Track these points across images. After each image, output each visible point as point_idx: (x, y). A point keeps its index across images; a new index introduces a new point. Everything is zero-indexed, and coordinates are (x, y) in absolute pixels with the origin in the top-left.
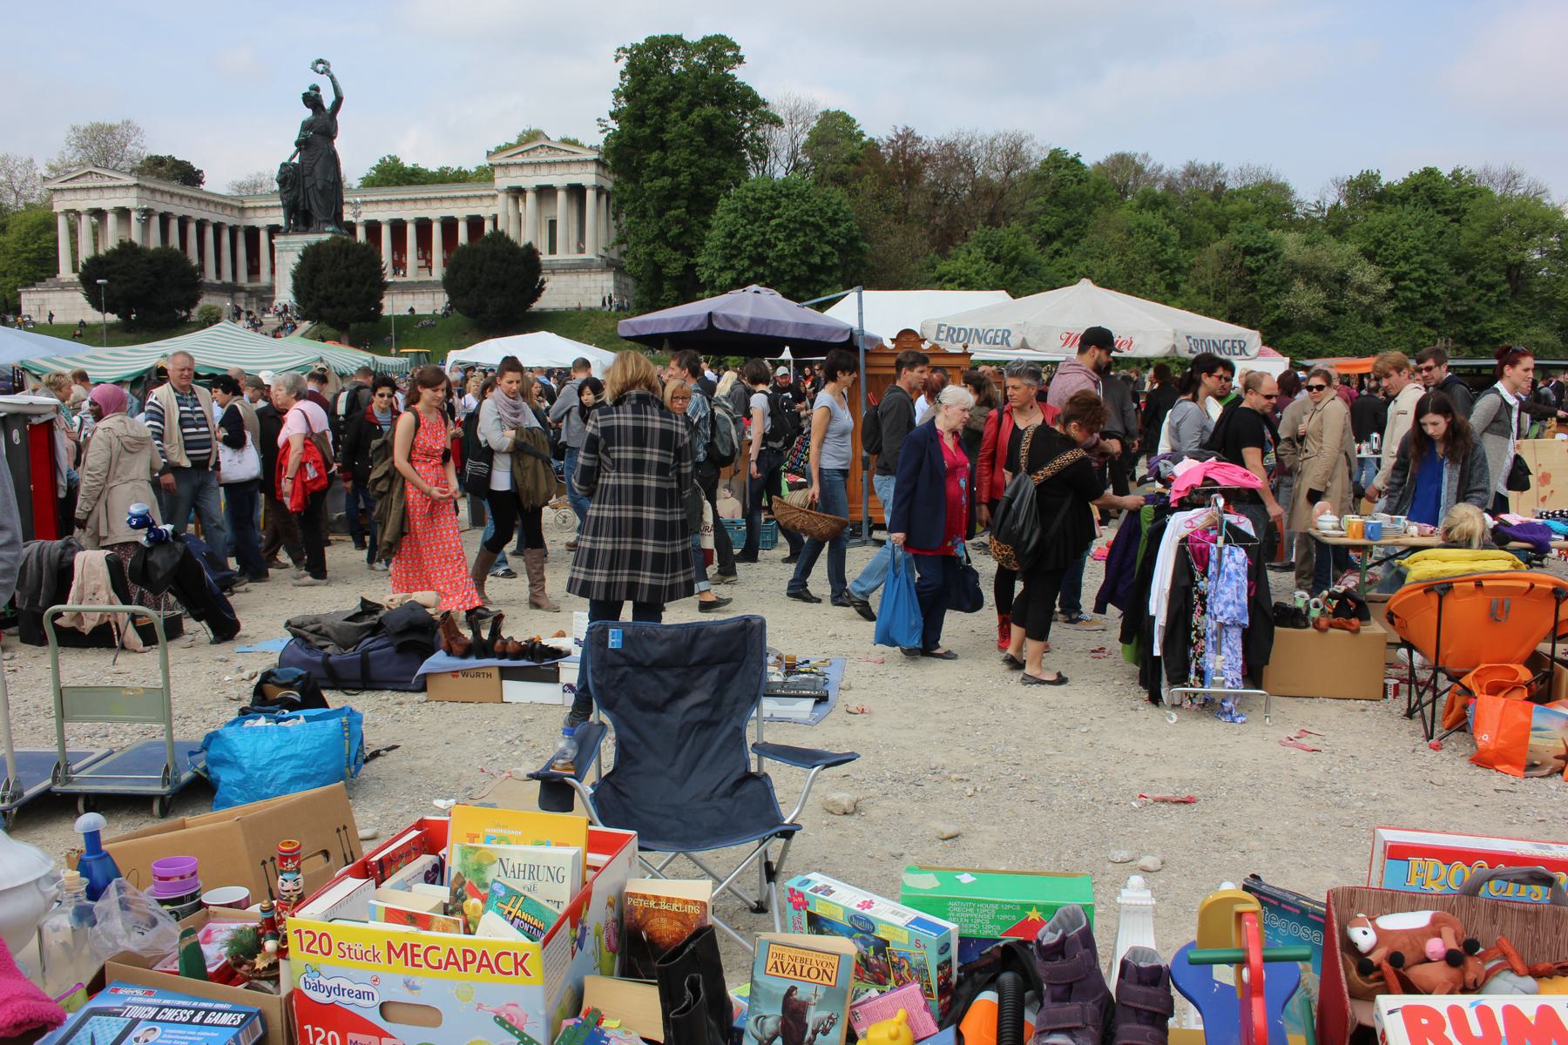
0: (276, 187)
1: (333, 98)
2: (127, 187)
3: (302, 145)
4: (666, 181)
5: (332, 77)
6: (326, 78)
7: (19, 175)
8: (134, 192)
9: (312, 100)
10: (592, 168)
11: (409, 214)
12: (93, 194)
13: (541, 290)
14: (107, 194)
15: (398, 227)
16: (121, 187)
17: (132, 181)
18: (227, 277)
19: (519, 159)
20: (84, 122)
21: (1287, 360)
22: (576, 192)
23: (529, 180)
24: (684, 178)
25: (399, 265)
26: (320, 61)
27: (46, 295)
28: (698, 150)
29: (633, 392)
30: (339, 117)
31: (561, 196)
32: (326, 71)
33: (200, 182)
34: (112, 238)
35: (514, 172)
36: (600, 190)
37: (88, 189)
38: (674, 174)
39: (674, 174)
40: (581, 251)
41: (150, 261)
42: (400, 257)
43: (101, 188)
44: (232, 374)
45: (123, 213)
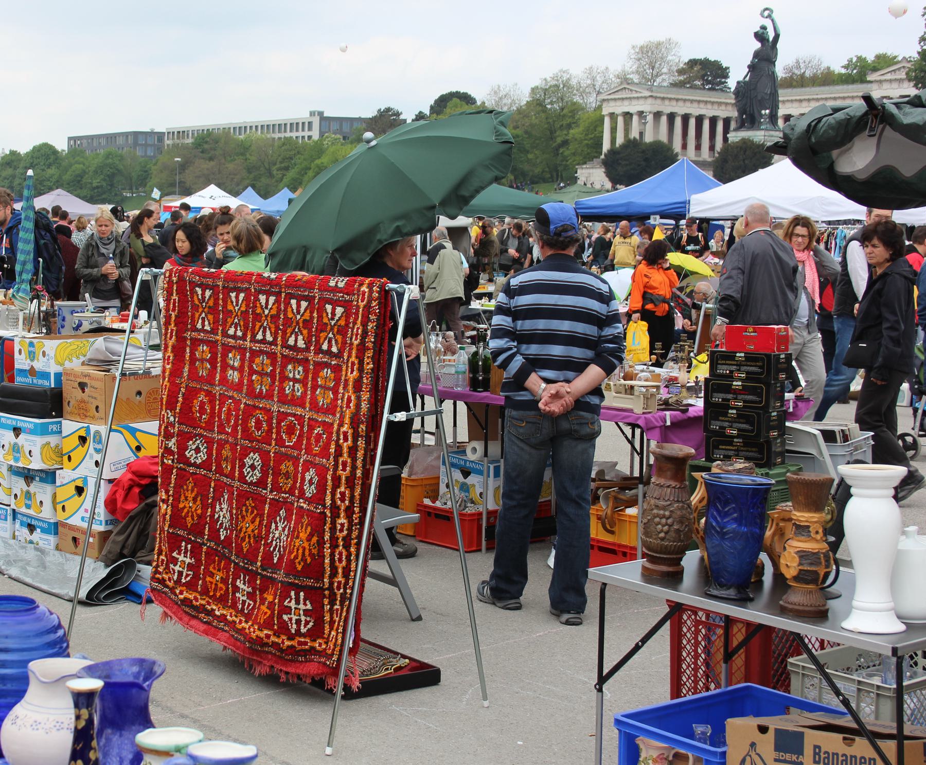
2: (646, 98)
3: (752, 67)
5: (773, 20)
8: (650, 101)
9: (760, 36)
12: (626, 103)
14: (634, 102)
16: (641, 97)
17: (647, 94)
19: (889, 77)
20: (641, 41)
26: (766, 9)
27: (591, 171)
30: (779, 46)
32: (769, 16)
34: (634, 134)
35: (886, 86)
37: (623, 99)
40: (124, 331)
41: (643, 152)
43: (630, 98)
45: (641, 114)
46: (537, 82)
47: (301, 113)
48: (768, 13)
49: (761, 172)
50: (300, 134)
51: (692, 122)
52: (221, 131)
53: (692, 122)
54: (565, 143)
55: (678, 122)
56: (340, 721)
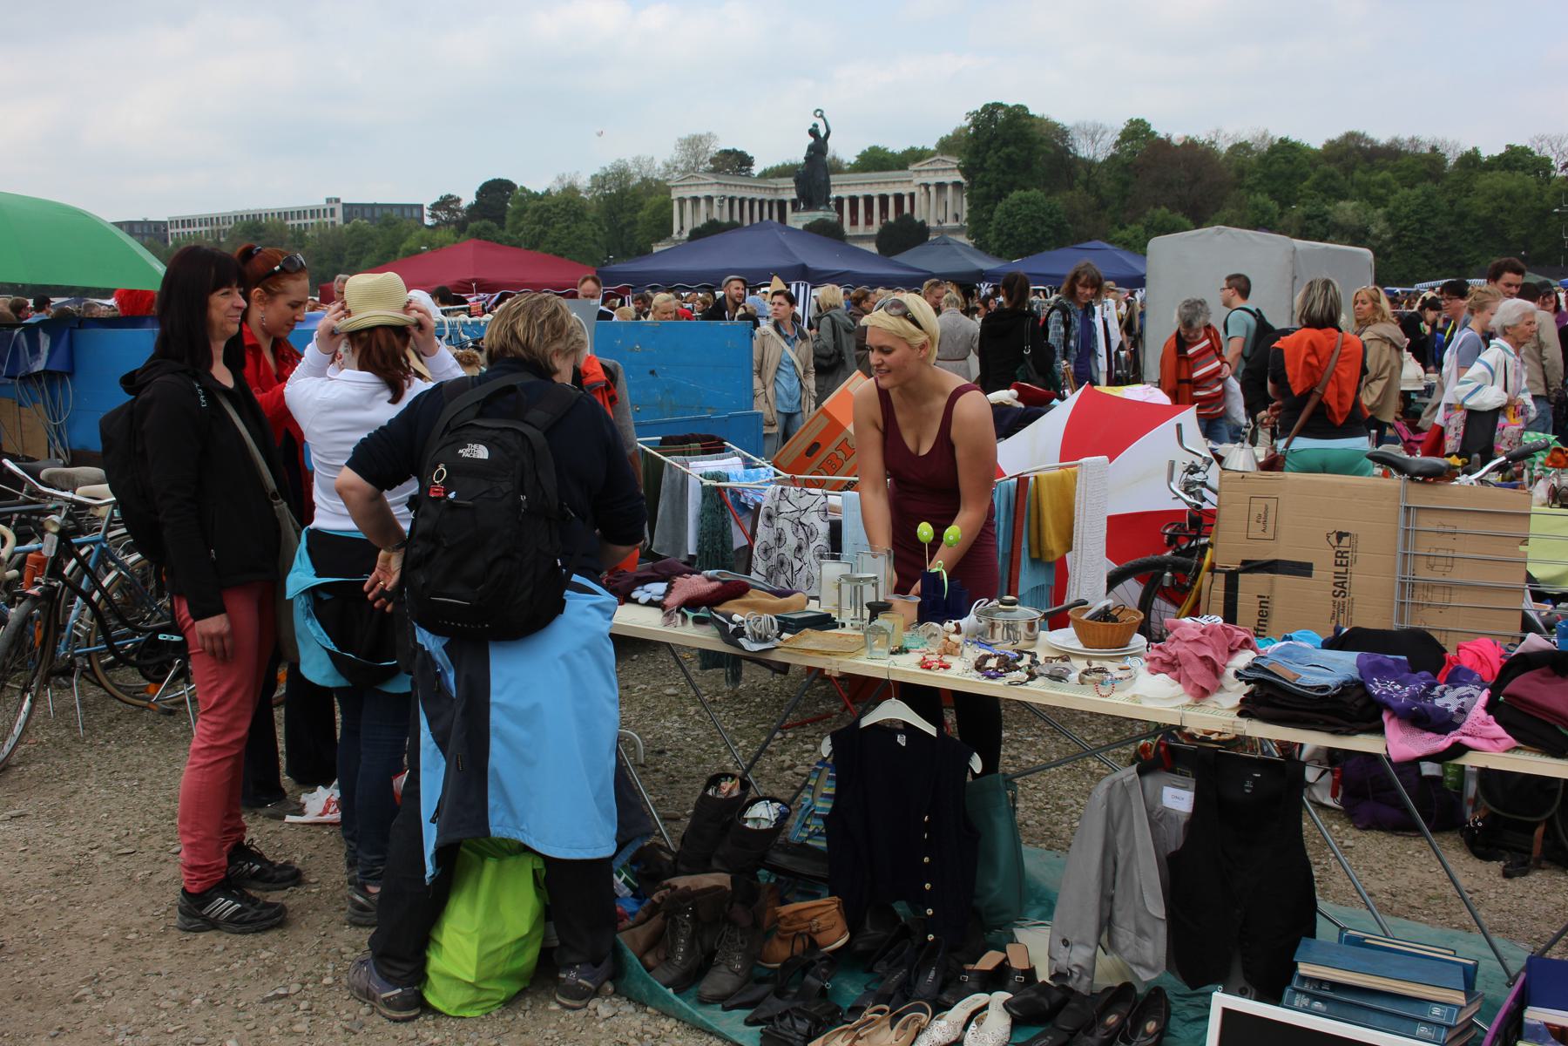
4: (985, 189)
7: (646, 167)
9: (814, 132)
11: (875, 192)
15: (854, 201)
20: (685, 135)
24: (993, 187)
25: (854, 222)
28: (1004, 172)
29: (56, 301)
31: (950, 188)
38: (989, 185)
39: (989, 185)
44: (1558, 678)
45: (709, 199)
46: (597, 171)
47: (319, 201)
49: (1381, 134)
50: (302, 221)
52: (1426, 151)
53: (747, 204)
54: (632, 223)
55: (737, 204)
56: (337, 829)
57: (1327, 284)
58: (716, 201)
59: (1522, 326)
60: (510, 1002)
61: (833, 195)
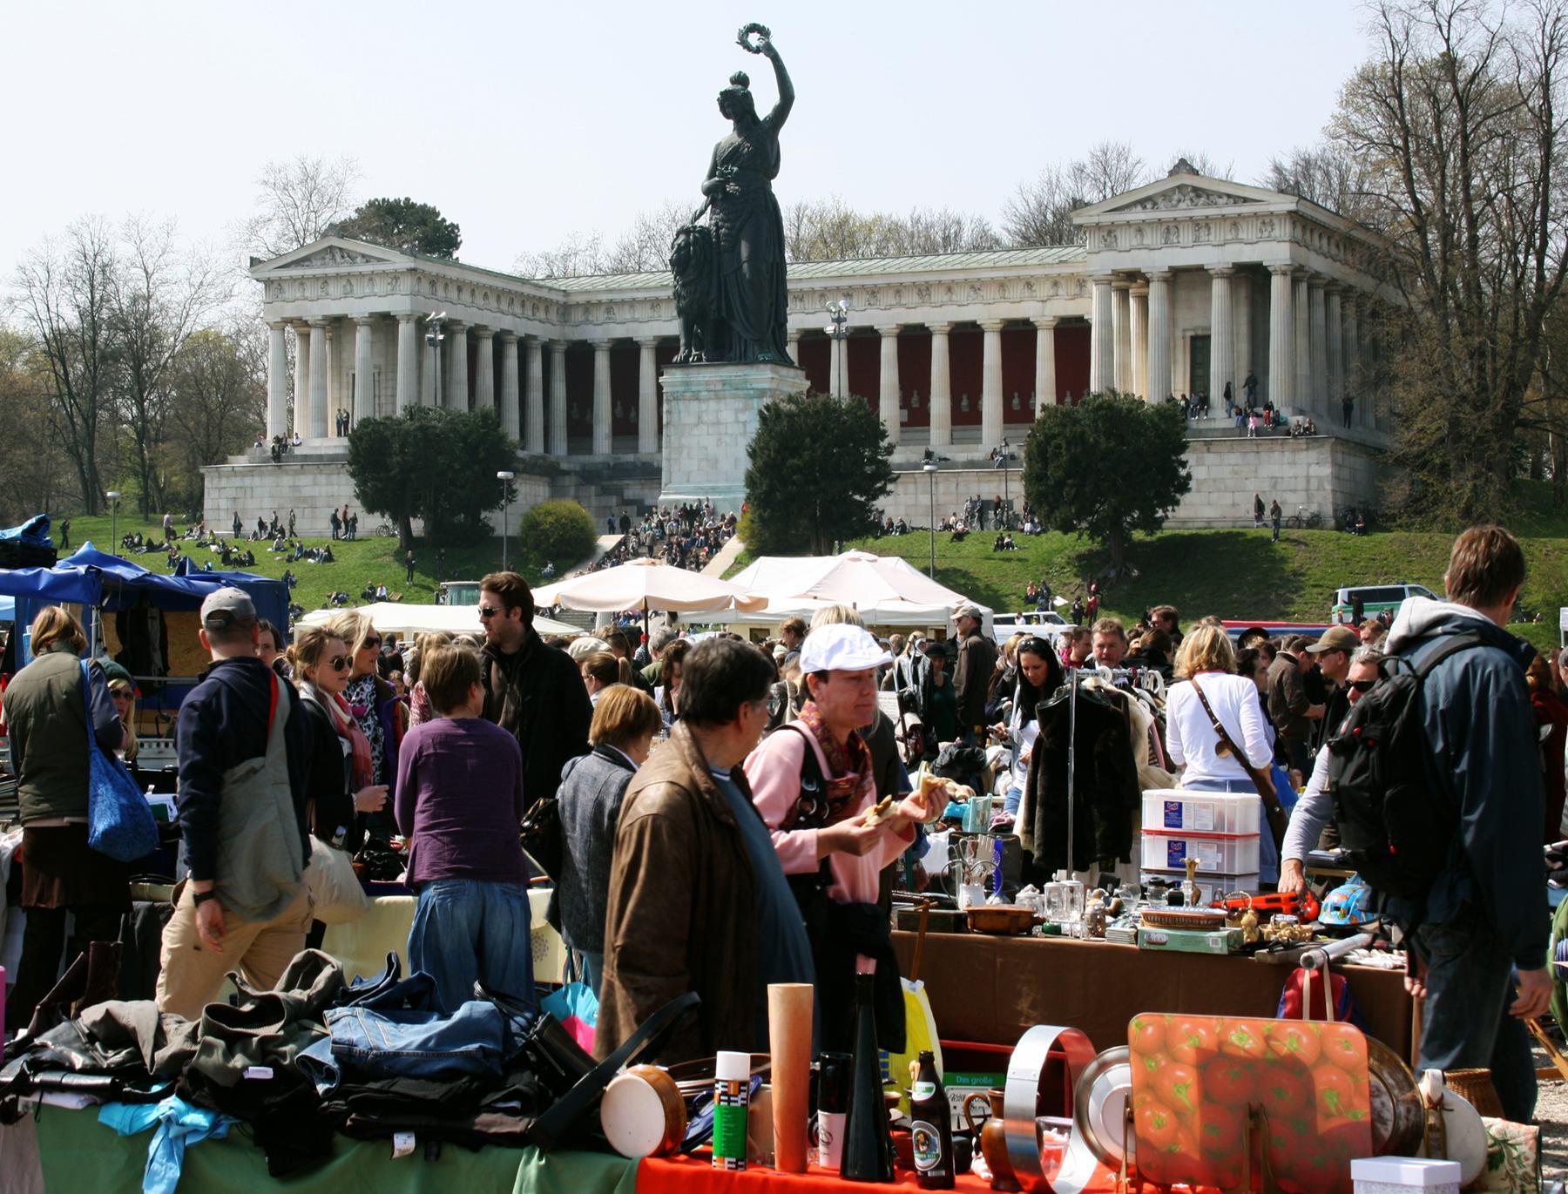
0: (669, 278)
1: (775, 99)
2: (395, 276)
6: (764, 61)
9: (736, 102)
10: (1283, 230)
13: (1183, 486)
18: (536, 447)
21: (808, 384)
22: (1252, 278)
23: (1157, 259)
25: (917, 417)
26: (754, 28)
30: (785, 136)
31: (1218, 288)
33: (454, 244)
36: (1297, 275)
37: (325, 280)
42: (626, 411)
45: (384, 324)
48: (756, 38)
51: (487, 348)
53: (487, 348)
57: (254, 262)
58: (405, 330)
59: (280, 498)
60: (1255, 1114)
61: (798, 320)
